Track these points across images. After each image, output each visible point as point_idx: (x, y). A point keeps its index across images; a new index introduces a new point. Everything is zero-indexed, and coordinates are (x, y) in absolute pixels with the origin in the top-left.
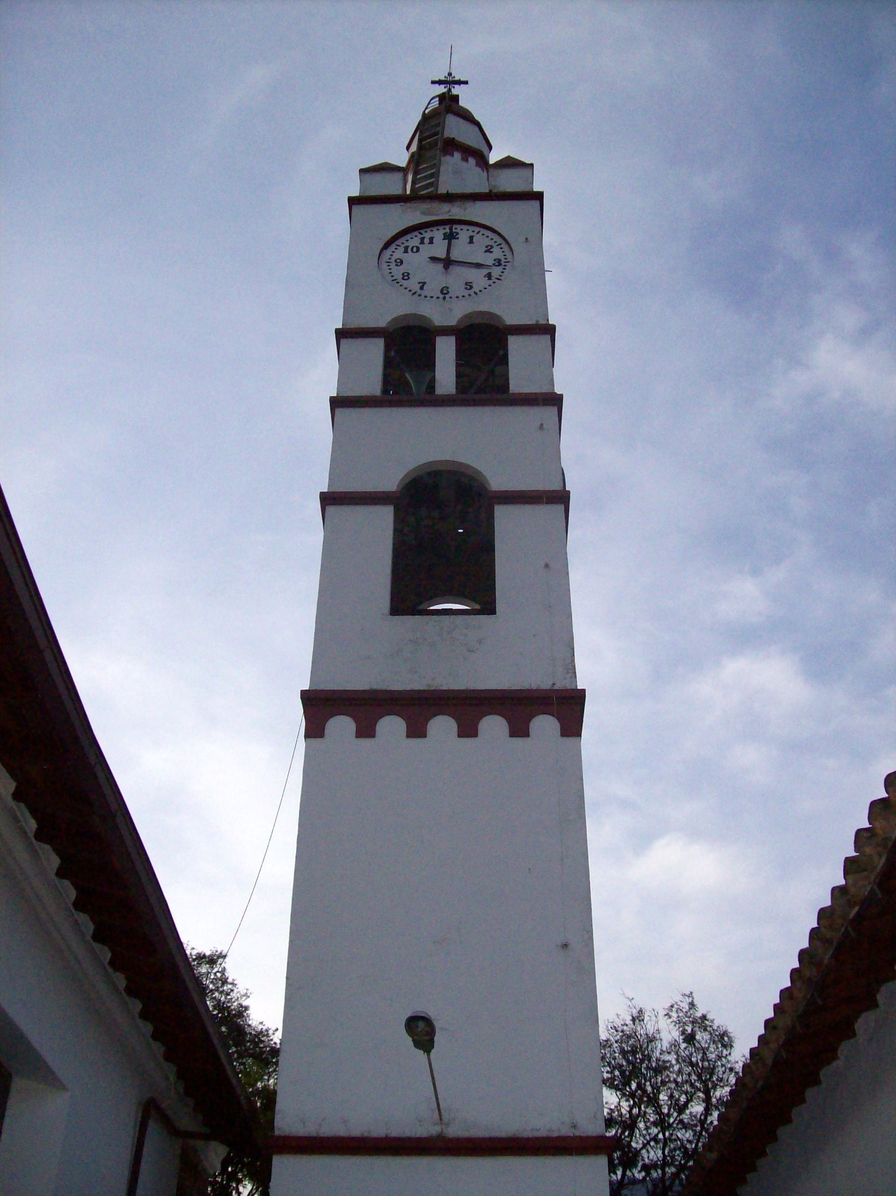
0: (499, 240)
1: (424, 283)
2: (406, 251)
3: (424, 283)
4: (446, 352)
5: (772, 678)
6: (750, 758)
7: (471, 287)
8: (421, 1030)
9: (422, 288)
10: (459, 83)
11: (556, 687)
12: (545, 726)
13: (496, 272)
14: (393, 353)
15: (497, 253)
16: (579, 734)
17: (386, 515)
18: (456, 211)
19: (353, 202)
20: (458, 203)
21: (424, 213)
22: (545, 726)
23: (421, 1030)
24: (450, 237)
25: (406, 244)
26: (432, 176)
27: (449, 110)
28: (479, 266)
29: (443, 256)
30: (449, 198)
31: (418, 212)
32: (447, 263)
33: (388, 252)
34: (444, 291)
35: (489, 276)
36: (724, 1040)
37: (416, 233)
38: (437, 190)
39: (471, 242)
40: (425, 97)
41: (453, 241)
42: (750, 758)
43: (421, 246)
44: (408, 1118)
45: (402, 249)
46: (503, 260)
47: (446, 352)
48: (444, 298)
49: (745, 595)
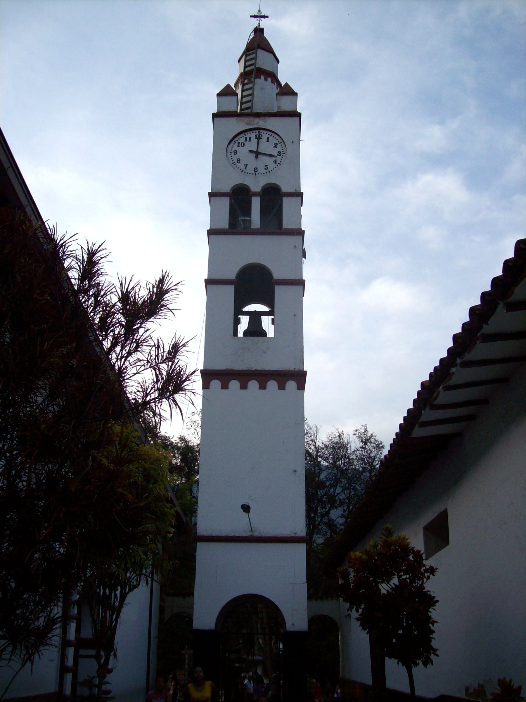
0: (281, 141)
1: (247, 165)
2: (238, 146)
3: (247, 165)
4: (256, 203)
5: (447, 187)
6: (431, 235)
7: (267, 168)
8: (246, 508)
9: (246, 168)
10: (264, 17)
11: (296, 370)
12: (291, 385)
13: (278, 159)
14: (233, 201)
15: (279, 148)
16: (304, 389)
17: (231, 289)
18: (260, 123)
19: (214, 116)
20: (262, 118)
21: (247, 124)
22: (291, 385)
23: (246, 508)
24: (259, 138)
25: (239, 141)
26: (251, 88)
27: (259, 47)
28: (271, 156)
29: (255, 150)
30: (258, 115)
31: (244, 123)
32: (257, 154)
33: (231, 146)
34: (255, 170)
35: (275, 162)
36: (379, 447)
37: (243, 135)
38: (252, 111)
39: (268, 141)
40: (245, 36)
41: (260, 140)
42: (431, 235)
43: (245, 143)
44: (241, 530)
45: (236, 144)
46: (282, 153)
47: (256, 203)
48: (255, 174)
49: (434, 136)
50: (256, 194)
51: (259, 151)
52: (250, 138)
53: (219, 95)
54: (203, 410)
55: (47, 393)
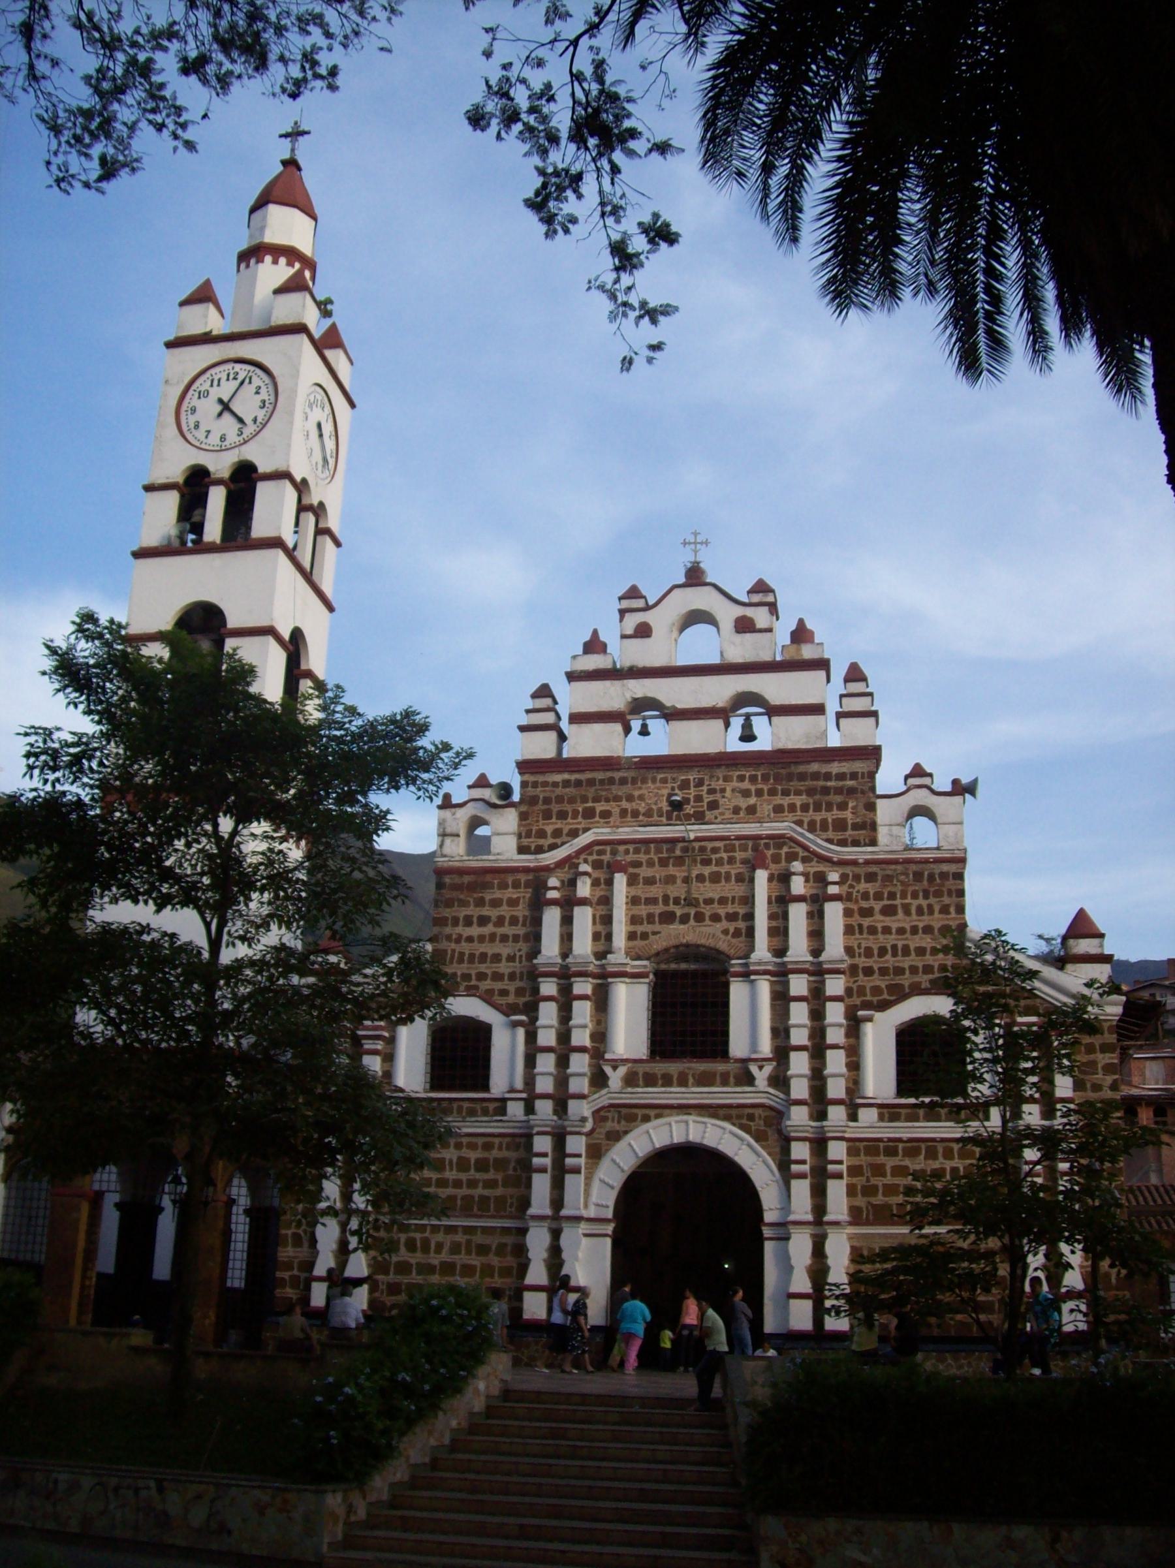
43: (210, 389)
50: (219, 482)
51: (232, 406)
52: (219, 380)
53: (749, 592)
54: (760, 1240)
55: (1085, 1315)
